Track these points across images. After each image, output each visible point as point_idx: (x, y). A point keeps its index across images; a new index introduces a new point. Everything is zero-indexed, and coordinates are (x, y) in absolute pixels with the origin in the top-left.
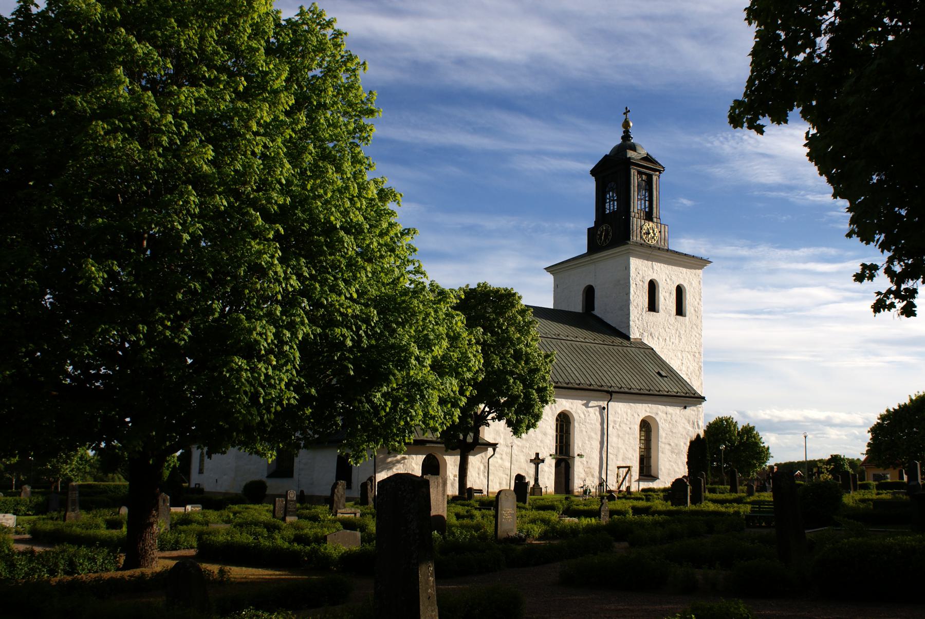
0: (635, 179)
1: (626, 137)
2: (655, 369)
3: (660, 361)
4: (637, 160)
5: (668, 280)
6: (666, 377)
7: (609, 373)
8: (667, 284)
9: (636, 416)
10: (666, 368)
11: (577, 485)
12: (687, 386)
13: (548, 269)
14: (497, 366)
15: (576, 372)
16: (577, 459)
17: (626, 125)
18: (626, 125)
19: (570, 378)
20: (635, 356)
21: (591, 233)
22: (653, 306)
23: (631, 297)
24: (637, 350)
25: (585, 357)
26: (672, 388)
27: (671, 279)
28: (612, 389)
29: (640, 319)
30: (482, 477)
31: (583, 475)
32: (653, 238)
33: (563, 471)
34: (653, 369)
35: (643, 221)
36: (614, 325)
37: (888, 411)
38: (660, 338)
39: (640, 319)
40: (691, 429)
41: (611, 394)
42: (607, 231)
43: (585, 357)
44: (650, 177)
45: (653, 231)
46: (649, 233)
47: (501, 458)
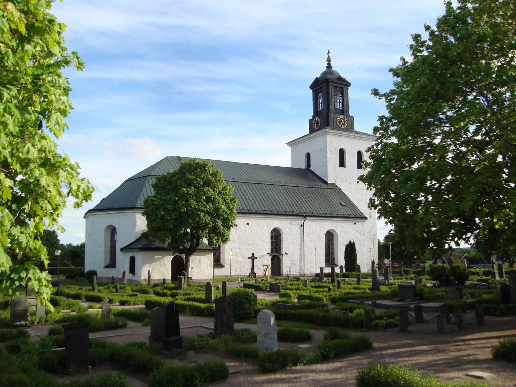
0: (332, 91)
1: (329, 67)
2: (339, 201)
4: (333, 80)
5: (352, 149)
6: (345, 206)
7: (307, 205)
8: (351, 151)
9: (323, 229)
12: (358, 211)
13: (289, 144)
14: (194, 206)
16: (285, 256)
17: (329, 60)
18: (329, 60)
19: (280, 208)
20: (328, 194)
21: (311, 122)
22: (342, 164)
23: (328, 159)
25: (294, 195)
26: (348, 212)
28: (307, 214)
30: (209, 268)
31: (289, 265)
32: (344, 124)
34: (336, 200)
38: (348, 183)
40: (359, 236)
41: (305, 216)
42: (317, 120)
44: (342, 88)
45: (344, 120)
46: (341, 121)
47: (236, 256)
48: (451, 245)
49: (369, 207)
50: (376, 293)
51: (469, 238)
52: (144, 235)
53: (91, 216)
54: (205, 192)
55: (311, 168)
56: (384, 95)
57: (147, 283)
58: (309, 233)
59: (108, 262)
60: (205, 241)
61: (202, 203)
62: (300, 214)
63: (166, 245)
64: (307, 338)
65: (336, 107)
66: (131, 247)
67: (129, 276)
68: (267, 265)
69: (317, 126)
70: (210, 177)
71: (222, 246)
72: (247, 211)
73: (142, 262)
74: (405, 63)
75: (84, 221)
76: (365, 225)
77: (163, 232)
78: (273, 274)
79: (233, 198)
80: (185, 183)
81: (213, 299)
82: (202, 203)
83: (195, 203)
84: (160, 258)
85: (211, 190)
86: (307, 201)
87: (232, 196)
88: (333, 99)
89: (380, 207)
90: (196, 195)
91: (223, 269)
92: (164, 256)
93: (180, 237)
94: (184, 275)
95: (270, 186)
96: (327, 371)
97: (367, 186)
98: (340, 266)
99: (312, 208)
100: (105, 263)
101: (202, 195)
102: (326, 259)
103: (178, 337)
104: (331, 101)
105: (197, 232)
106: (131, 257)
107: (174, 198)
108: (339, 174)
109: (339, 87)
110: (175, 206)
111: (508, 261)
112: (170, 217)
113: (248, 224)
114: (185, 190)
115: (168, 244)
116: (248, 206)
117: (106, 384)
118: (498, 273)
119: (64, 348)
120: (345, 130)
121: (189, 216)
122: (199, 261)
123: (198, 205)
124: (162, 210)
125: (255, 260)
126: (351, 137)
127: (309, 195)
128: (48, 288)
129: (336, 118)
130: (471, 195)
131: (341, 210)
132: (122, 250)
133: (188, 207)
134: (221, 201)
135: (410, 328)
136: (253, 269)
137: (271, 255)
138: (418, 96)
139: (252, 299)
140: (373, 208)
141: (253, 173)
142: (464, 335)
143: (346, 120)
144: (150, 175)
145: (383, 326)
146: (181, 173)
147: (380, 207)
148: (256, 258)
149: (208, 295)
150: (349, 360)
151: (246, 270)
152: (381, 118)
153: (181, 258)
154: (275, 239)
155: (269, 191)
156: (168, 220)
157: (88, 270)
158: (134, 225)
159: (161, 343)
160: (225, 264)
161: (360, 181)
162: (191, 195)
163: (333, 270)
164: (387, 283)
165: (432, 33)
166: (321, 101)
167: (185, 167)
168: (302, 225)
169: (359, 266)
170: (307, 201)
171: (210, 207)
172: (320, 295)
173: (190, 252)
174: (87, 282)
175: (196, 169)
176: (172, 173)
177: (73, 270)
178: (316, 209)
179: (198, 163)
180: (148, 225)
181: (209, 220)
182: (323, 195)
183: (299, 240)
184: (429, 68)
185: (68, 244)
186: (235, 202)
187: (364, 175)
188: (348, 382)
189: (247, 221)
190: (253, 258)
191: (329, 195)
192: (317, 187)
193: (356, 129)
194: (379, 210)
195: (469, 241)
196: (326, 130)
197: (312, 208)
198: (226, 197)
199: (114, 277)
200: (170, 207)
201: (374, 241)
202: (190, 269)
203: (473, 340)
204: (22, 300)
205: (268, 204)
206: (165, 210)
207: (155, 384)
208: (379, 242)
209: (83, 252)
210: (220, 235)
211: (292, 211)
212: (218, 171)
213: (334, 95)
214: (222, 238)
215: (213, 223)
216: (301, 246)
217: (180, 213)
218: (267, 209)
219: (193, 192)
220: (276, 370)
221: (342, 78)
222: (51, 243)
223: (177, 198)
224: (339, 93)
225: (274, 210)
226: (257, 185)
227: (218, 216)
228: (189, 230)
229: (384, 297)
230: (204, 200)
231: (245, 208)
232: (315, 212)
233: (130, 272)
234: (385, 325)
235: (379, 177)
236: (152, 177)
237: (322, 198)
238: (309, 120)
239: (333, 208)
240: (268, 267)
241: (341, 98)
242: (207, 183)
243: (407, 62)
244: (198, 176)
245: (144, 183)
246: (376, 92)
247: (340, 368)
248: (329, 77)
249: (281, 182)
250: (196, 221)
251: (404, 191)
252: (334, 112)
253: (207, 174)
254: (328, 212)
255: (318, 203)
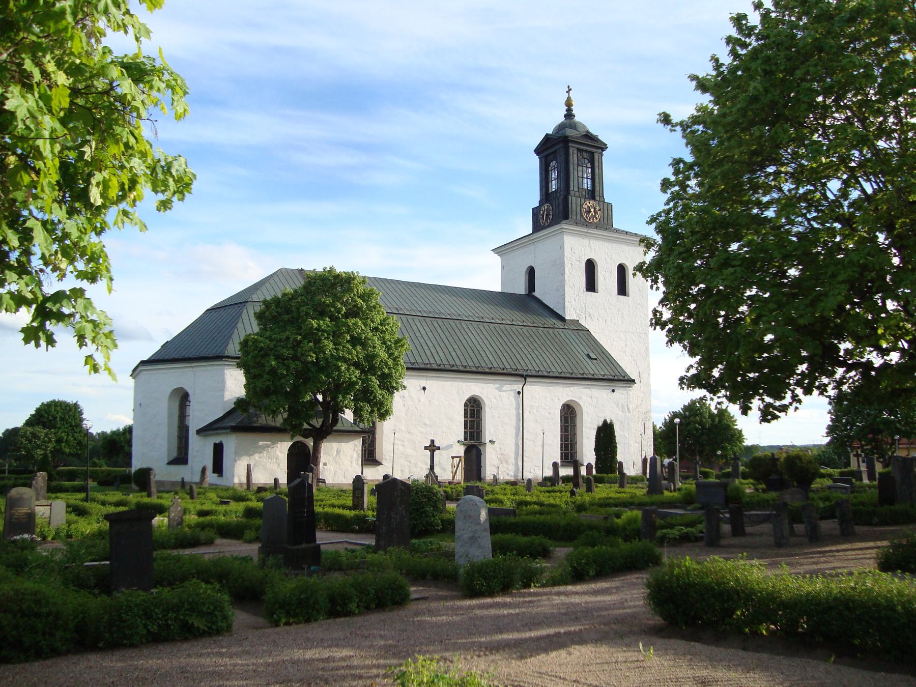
0: (574, 157)
1: (569, 115)
2: (585, 351)
3: (593, 343)
4: (576, 138)
5: (608, 259)
7: (529, 356)
10: (599, 350)
11: (489, 472)
12: (619, 369)
13: (497, 251)
15: (490, 356)
16: (489, 445)
17: (569, 104)
18: (569, 104)
19: (482, 362)
21: (536, 212)
22: (591, 286)
23: (566, 277)
24: (570, 332)
25: (506, 340)
26: (600, 370)
27: (611, 258)
28: (529, 373)
29: (577, 299)
30: (354, 464)
31: (496, 462)
33: (474, 457)
34: (581, 350)
35: (583, 200)
36: (551, 307)
37: (684, 406)
38: (600, 319)
39: (577, 299)
40: (620, 413)
41: (525, 377)
42: (548, 210)
43: (506, 340)
44: (592, 154)
45: (595, 209)
46: (590, 212)
48: (796, 392)
49: (651, 325)
50: (656, 498)
51: (826, 385)
52: (240, 404)
53: (144, 373)
54: (349, 326)
55: (536, 294)
56: (681, 124)
57: (245, 487)
58: (532, 407)
59: (175, 454)
60: (348, 415)
61: (344, 347)
62: (518, 372)
63: (279, 421)
64: (545, 554)
65: (580, 186)
66: (218, 425)
67: (211, 477)
68: (460, 457)
69: (546, 220)
70: (359, 300)
71: (378, 424)
72: (423, 366)
73: (236, 453)
74: (718, 65)
75: (132, 381)
76: (631, 393)
77: (274, 398)
78: (467, 479)
79: (398, 339)
80: (315, 310)
81: (365, 506)
82: (344, 347)
83: (331, 346)
84: (268, 446)
85: (360, 323)
86: (530, 350)
87: (396, 336)
88: (576, 172)
89: (671, 326)
90: (334, 332)
91: (379, 468)
92: (274, 443)
93: (304, 407)
94: (312, 470)
95: (463, 323)
96: (584, 593)
97: (649, 283)
98: (585, 464)
99: (538, 362)
100: (168, 456)
101: (343, 333)
102: (561, 453)
103: (312, 545)
104: (572, 176)
105: (334, 398)
106: (215, 444)
107: (294, 336)
108: (585, 304)
109: (587, 151)
110: (296, 351)
111: (881, 460)
112: (287, 371)
113: (424, 388)
114: (314, 323)
115: (282, 421)
116: (424, 358)
117: (191, 600)
118: (866, 473)
119: (108, 562)
120: (597, 226)
121: (321, 370)
122: (338, 452)
123: (337, 349)
124: (272, 357)
125: (437, 452)
126: (607, 239)
127: (532, 340)
128: (109, 340)
129: (581, 206)
130: (838, 286)
131: (588, 367)
132: (199, 432)
133: (320, 352)
134: (378, 343)
135: (723, 542)
136: (432, 468)
137: (464, 444)
138: (744, 116)
139: (439, 498)
140: (658, 327)
141: (433, 301)
142: (823, 546)
143: (598, 208)
144: (250, 300)
145: (675, 539)
146: (308, 293)
147: (671, 326)
148: (439, 448)
149: (358, 498)
150: (624, 580)
151: (419, 470)
152: (677, 162)
153: (305, 446)
154: (472, 415)
155: (462, 331)
156: (285, 376)
157: (138, 467)
158: (222, 388)
159: (281, 556)
160: (382, 459)
161: (638, 273)
162: (324, 331)
163: (577, 471)
164: (672, 488)
165: (765, 16)
166: (554, 175)
167: (315, 283)
168: (519, 393)
169: (621, 464)
170: (530, 350)
171: (358, 353)
172: (558, 501)
173: (321, 434)
174: (137, 488)
175: (333, 286)
176: (291, 294)
177: (109, 473)
178: (545, 364)
179: (338, 276)
180: (247, 386)
181: (356, 377)
182: (557, 340)
183: (514, 419)
184: (763, 67)
185: (99, 432)
186: (402, 346)
187: (644, 263)
188: (626, 604)
189: (423, 383)
190: (432, 448)
191: (567, 341)
192: (546, 326)
193: (616, 225)
194: (669, 331)
195: (827, 392)
196: (564, 225)
197: (538, 362)
198: (387, 337)
199: (185, 480)
200: (286, 352)
201: (647, 423)
202: (321, 465)
203: (838, 551)
204: (25, 496)
205: (459, 353)
206: (278, 357)
207: (276, 606)
208: (654, 427)
209: (129, 443)
210: (376, 404)
211: (502, 366)
212: (372, 290)
213: (578, 165)
214: (379, 410)
215: (363, 382)
216: (517, 428)
217: (305, 363)
218: (458, 363)
219: (328, 326)
220: (494, 592)
221: (591, 134)
222: (71, 426)
223: (299, 338)
224: (586, 161)
225: (471, 364)
226: (440, 321)
227: (372, 369)
228: (320, 397)
229: (671, 504)
230: (348, 341)
231: (419, 360)
232: (542, 369)
233: (214, 472)
234: (678, 537)
235: (673, 263)
236: (254, 303)
237: (555, 345)
238: (533, 209)
239: (575, 363)
240: (460, 460)
241: (590, 170)
242: (354, 312)
243: (723, 64)
244: (337, 298)
245: (239, 315)
246: (666, 119)
247: (608, 589)
248: (569, 132)
249: (482, 316)
250: (333, 379)
251: (721, 281)
252: (577, 193)
253: (354, 295)
254: (567, 370)
255: (548, 354)
